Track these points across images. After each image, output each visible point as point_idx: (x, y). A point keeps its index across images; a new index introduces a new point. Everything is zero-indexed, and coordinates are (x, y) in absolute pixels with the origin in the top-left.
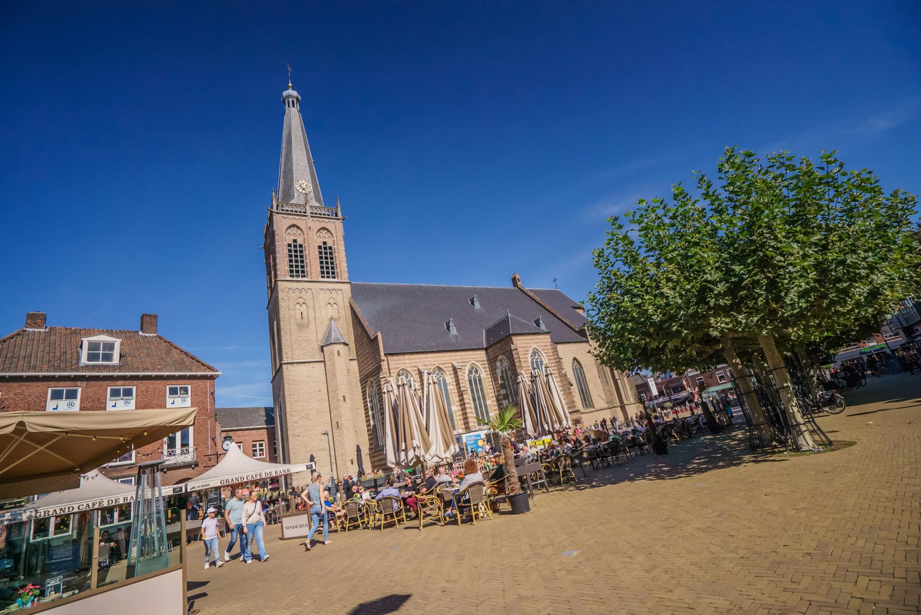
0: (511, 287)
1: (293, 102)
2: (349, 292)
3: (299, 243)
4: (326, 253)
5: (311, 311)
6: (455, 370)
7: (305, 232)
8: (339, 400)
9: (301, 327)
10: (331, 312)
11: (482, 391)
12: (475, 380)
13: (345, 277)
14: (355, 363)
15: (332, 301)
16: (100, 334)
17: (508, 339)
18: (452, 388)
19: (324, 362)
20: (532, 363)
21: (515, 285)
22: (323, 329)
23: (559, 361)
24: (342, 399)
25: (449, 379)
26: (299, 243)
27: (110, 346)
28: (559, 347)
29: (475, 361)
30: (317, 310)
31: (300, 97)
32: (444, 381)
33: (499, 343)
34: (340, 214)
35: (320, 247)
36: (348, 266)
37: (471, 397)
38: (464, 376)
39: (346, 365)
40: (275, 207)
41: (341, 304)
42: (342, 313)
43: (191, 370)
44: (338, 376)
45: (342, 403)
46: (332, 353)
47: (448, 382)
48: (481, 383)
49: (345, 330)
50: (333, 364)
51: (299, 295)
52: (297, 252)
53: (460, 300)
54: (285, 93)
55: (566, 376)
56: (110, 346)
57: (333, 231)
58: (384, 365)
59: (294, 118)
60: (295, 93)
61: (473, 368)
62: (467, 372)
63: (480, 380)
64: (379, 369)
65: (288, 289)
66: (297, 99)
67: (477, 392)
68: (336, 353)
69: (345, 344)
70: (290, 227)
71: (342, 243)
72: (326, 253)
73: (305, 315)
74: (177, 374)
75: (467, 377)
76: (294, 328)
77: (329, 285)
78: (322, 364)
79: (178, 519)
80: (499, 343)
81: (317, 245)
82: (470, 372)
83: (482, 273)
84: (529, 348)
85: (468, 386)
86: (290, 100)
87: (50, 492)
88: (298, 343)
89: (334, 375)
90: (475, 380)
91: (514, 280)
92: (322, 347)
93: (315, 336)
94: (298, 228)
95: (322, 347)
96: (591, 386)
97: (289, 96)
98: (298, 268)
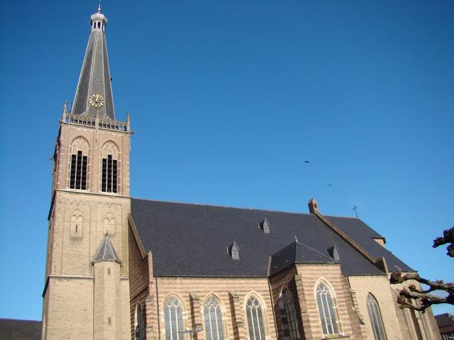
0: (307, 211)
1: (99, 23)
2: (129, 207)
4: (110, 167)
6: (231, 298)
7: (91, 144)
8: (103, 322)
9: (75, 239)
10: (108, 227)
11: (262, 324)
12: (254, 311)
13: (127, 192)
14: (126, 284)
15: (110, 216)
17: (292, 267)
18: (227, 319)
19: (94, 279)
20: (318, 296)
21: (312, 210)
22: (96, 244)
23: (350, 296)
24: (106, 321)
25: (224, 308)
26: (113, 159)
28: (352, 279)
29: (257, 291)
30: (93, 224)
31: (106, 20)
32: (219, 311)
33: (282, 275)
34: (128, 128)
35: (104, 160)
36: (131, 182)
37: (247, 331)
38: (242, 307)
39: (116, 284)
40: (64, 118)
41: (119, 220)
42: (120, 229)
44: (106, 295)
45: (106, 325)
46: (102, 271)
47: (222, 312)
48: (260, 315)
49: (121, 246)
50: (102, 283)
51: (76, 207)
52: (80, 163)
53: (242, 223)
54: (93, 17)
55: (356, 312)
57: (120, 144)
58: (152, 288)
60: (102, 16)
61: (252, 298)
62: (245, 302)
63: (260, 311)
64: (146, 290)
65: (68, 198)
66: (104, 21)
67: (256, 325)
68: (106, 271)
69: (118, 262)
71: (128, 157)
72: (110, 167)
73: (79, 228)
74: (84, 61)
75: (244, 308)
76: (67, 241)
77: (109, 198)
78: (91, 283)
80: (282, 275)
81: (101, 158)
82: (249, 303)
83: (275, 192)
84: (317, 280)
85: (245, 317)
86: (97, 22)
88: (71, 257)
89: (101, 294)
90: (254, 311)
91: (311, 206)
93: (89, 248)
96: (387, 325)
97: (98, 19)
98: (79, 179)
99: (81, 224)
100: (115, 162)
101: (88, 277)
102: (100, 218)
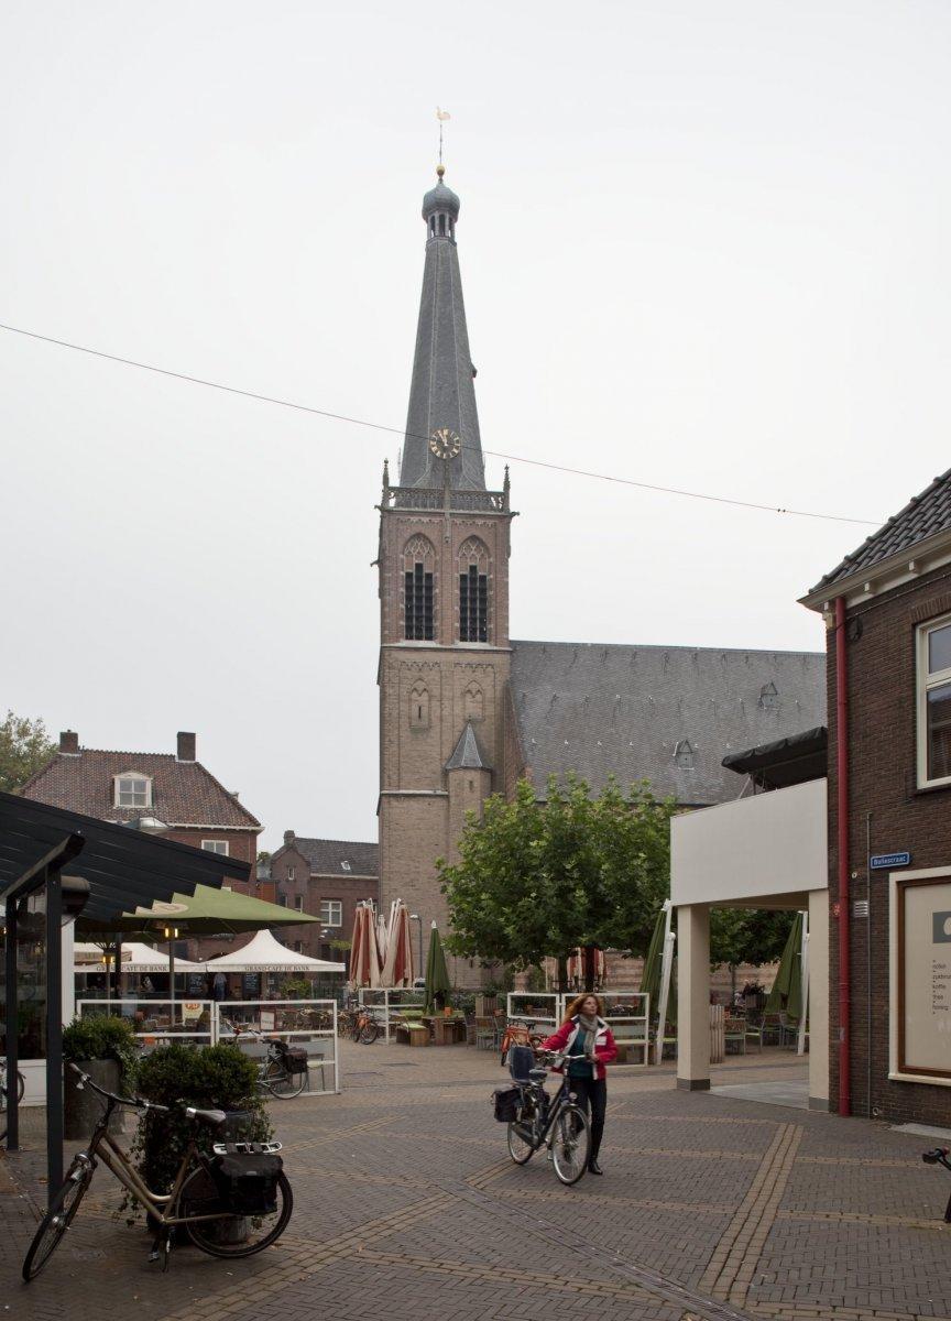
3: (426, 570)
5: (435, 703)
7: (438, 549)
15: (474, 687)
16: (907, 1122)
26: (426, 570)
27: (141, 786)
30: (446, 703)
35: (463, 577)
41: (489, 694)
43: (228, 823)
56: (141, 786)
59: (141, 912)
70: (412, 537)
79: (155, 1174)
81: (457, 575)
87: (508, 541)
92: (446, 773)
94: (426, 538)
95: (446, 773)
99: (426, 704)
100: (483, 578)
101: (439, 792)
102: (458, 694)
